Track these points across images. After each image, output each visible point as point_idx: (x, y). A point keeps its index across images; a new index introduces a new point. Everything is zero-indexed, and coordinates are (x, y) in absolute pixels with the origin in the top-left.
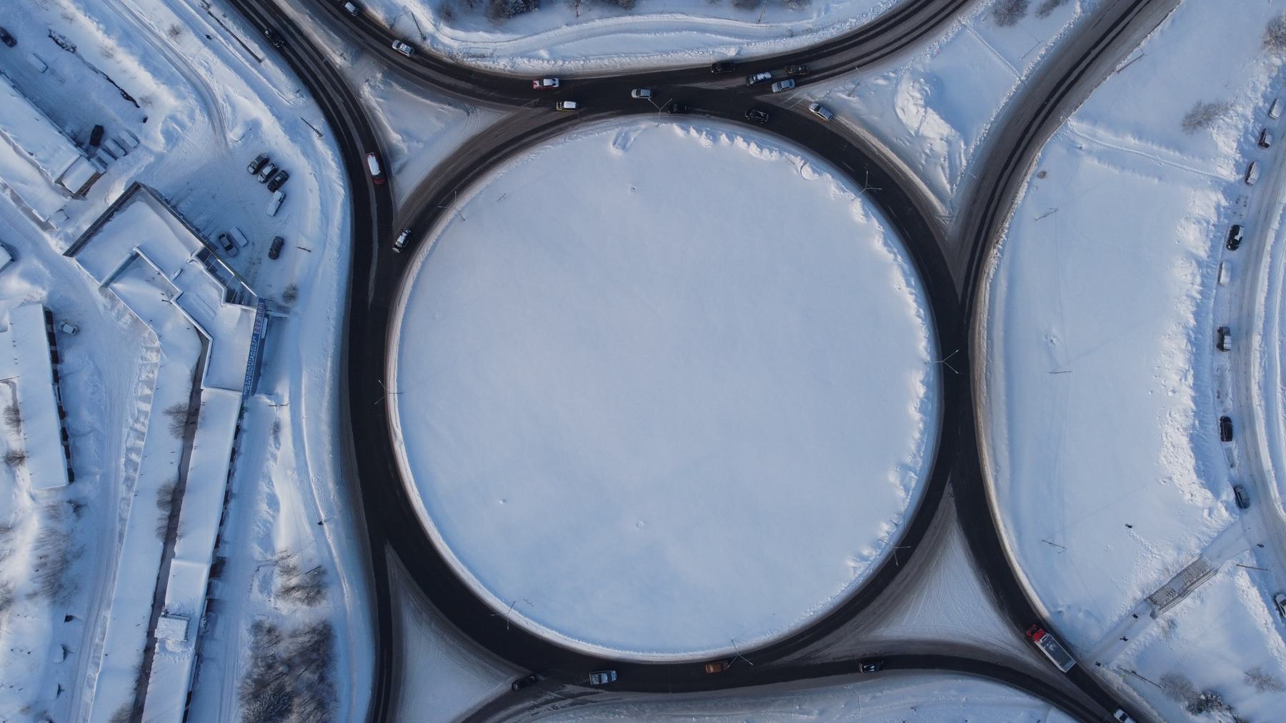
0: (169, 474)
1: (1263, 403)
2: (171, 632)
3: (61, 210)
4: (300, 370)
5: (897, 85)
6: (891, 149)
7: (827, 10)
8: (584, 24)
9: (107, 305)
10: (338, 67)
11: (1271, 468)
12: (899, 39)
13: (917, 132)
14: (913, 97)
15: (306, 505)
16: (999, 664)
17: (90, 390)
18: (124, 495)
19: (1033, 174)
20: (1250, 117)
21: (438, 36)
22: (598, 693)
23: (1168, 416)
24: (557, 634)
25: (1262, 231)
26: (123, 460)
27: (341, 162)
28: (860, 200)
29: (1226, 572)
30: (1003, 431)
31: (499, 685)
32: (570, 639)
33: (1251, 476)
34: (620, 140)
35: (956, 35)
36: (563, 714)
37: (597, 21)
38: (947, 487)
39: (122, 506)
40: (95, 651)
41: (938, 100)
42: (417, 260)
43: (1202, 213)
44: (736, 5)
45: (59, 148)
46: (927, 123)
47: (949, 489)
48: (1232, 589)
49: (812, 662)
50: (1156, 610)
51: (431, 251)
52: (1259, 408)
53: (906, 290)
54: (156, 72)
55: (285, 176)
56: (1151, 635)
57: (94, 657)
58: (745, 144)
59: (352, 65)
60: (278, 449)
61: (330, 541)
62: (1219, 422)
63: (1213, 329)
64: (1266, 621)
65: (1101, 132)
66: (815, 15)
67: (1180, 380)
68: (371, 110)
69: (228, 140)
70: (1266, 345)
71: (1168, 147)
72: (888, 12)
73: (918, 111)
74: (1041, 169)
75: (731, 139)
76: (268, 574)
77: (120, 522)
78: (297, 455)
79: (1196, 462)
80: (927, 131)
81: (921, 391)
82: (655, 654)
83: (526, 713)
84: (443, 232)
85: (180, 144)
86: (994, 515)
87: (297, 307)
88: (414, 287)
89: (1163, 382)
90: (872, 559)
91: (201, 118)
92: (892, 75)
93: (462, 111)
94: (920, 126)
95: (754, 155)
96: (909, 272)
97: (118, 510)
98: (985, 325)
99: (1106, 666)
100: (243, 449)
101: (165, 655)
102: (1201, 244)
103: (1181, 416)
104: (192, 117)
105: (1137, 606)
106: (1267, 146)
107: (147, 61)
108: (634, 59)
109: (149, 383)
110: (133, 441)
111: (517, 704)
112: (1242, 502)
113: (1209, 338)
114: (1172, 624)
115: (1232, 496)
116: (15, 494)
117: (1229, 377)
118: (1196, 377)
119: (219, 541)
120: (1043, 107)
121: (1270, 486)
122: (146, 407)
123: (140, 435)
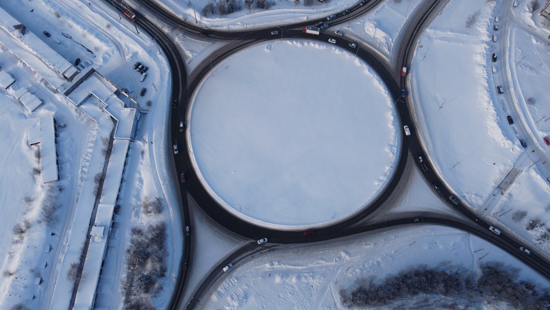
0: (99, 170)
1: (521, 110)
2: (98, 233)
3: (62, 85)
4: (152, 130)
5: (364, 24)
6: (366, 42)
7: (336, 4)
8: (253, 14)
9: (77, 116)
10: (166, 33)
11: (531, 132)
12: (362, 11)
13: (374, 37)
14: (370, 26)
15: (154, 179)
16: (445, 218)
17: (69, 146)
18: (80, 184)
19: (418, 47)
20: (488, 22)
21: (202, 22)
22: (279, 245)
23: (487, 118)
24: (260, 221)
25: (504, 56)
26: (80, 171)
27: (169, 66)
28: (357, 58)
29: (525, 171)
30: (425, 127)
31: (237, 246)
32: (265, 223)
33: (525, 136)
34: (268, 47)
35: (382, 7)
36: (265, 255)
37: (257, 13)
38: (409, 152)
39: (79, 188)
40: (63, 248)
41: (379, 25)
42: (197, 90)
43: (480, 51)
44: (305, 5)
45: (64, 63)
46: (377, 33)
47: (410, 153)
48: (530, 177)
49: (367, 224)
50: (503, 191)
51: (202, 87)
52: (520, 112)
53: (379, 85)
54: (101, 39)
55: (147, 69)
56: (503, 201)
57: (62, 251)
58: (314, 45)
59: (171, 32)
60: (143, 160)
61: (164, 192)
62: (507, 118)
63: (495, 87)
64: (547, 188)
65: (438, 32)
66: (332, 6)
67: (488, 104)
68: (178, 45)
69: (126, 59)
70: (516, 91)
71: (463, 33)
72: (357, 3)
73: (373, 30)
74: (421, 45)
75: (309, 44)
76: (138, 210)
77: (77, 194)
78: (151, 161)
79: (502, 131)
80: (376, 36)
81: (392, 118)
82: (301, 226)
83: (249, 256)
84: (206, 81)
85: (108, 62)
86: (429, 161)
87: (152, 109)
88: (196, 99)
89: (482, 107)
90: (384, 181)
91: (116, 52)
92: (362, 21)
93: (211, 43)
94: (375, 34)
95: (317, 48)
96: (379, 80)
97: (77, 190)
98: (411, 95)
99: (489, 215)
100: (129, 162)
101: (94, 243)
102: (483, 61)
103: (492, 116)
104: (113, 52)
105: (495, 190)
106: (497, 29)
107: (97, 36)
108: (271, 23)
109: (92, 142)
110: (85, 163)
111: (245, 253)
112: (524, 144)
113: (495, 91)
114: (510, 195)
115: (520, 143)
116: (35, 187)
117: (506, 103)
118: (493, 102)
119: (118, 198)
120: (416, 27)
121: (533, 140)
122: (91, 150)
123: (88, 161)
